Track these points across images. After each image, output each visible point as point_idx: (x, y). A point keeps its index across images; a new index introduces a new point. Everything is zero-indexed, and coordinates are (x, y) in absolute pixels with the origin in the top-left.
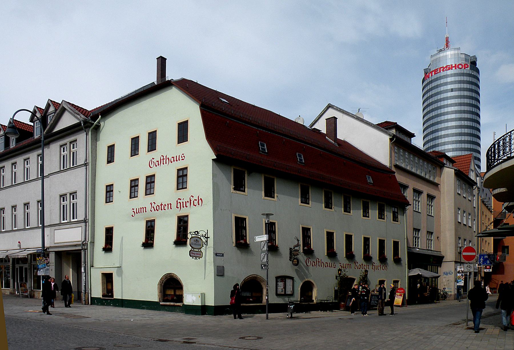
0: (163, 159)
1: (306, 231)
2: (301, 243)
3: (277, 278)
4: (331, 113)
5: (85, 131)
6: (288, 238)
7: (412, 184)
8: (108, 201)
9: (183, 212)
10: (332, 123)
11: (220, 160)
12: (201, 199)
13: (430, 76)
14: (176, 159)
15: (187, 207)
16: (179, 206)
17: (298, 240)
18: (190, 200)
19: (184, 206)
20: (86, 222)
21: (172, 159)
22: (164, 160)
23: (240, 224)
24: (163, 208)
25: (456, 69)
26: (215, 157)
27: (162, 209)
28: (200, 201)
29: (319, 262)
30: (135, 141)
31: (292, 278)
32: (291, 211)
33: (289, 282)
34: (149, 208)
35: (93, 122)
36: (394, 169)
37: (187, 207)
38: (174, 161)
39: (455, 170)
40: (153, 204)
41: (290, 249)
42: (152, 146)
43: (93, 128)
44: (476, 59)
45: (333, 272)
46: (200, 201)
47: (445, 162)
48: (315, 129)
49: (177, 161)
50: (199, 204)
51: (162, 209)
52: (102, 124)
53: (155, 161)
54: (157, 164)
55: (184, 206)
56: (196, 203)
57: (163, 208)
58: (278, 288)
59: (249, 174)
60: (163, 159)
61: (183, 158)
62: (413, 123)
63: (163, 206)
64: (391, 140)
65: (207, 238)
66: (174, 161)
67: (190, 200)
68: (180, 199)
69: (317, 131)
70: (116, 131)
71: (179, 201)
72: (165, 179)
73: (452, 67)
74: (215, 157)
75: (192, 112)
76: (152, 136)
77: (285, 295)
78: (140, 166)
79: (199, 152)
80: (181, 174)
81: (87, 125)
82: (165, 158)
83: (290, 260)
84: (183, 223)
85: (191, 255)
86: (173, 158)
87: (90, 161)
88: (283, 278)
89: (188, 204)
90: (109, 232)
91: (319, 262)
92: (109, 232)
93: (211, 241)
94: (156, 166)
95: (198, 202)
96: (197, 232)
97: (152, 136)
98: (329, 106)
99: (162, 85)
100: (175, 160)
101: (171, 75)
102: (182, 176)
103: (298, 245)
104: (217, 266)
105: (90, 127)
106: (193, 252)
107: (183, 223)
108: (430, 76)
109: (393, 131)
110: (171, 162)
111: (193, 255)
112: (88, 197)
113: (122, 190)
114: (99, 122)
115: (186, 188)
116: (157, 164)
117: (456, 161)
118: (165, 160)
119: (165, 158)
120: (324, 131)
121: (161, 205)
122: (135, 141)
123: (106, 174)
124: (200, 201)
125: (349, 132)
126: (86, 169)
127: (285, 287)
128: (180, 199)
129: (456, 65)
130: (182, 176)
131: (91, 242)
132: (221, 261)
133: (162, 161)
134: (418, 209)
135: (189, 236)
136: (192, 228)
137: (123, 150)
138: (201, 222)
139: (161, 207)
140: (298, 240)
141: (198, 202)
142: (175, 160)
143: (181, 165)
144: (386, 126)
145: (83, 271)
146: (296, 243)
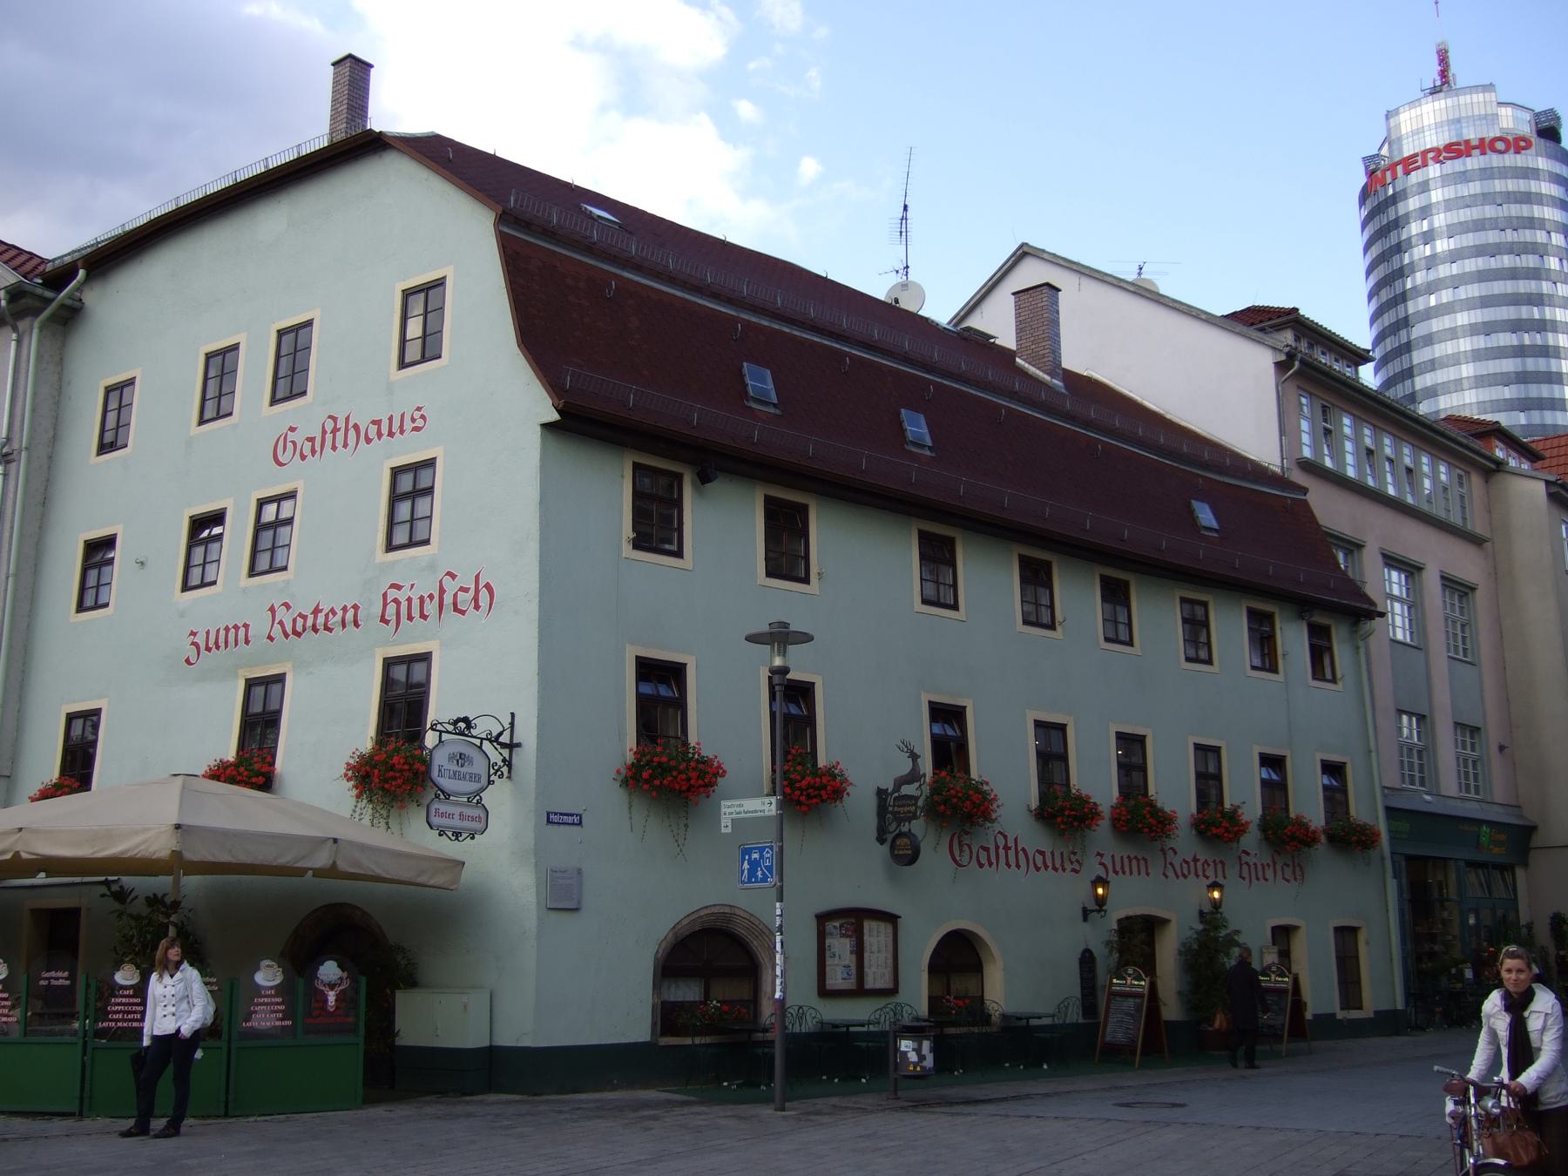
0: (335, 431)
1: (947, 715)
3: (823, 918)
4: (1030, 275)
5: (15, 329)
6: (871, 742)
8: (89, 602)
10: (1039, 306)
11: (576, 423)
12: (488, 586)
13: (1389, 179)
14: (387, 429)
15: (424, 617)
16: (392, 608)
17: (914, 757)
18: (442, 591)
21: (373, 429)
22: (339, 433)
23: (661, 683)
26: (554, 416)
28: (482, 594)
29: (1007, 848)
30: (221, 364)
31: (891, 919)
32: (888, 633)
33: (877, 936)
34: (261, 627)
35: (48, 294)
36: (1298, 477)
37: (424, 617)
38: (380, 435)
39: (1548, 483)
40: (281, 613)
41: (881, 793)
42: (289, 381)
45: (1072, 889)
46: (484, 594)
47: (1499, 453)
48: (969, 329)
49: (391, 434)
50: (477, 607)
52: (91, 297)
53: (298, 437)
54: (307, 451)
58: (829, 961)
59: (704, 478)
60: (335, 431)
61: (419, 423)
62: (1351, 319)
64: (1281, 367)
65: (511, 746)
66: (380, 435)
67: (442, 591)
68: (398, 587)
69: (980, 343)
70: (150, 331)
71: (392, 594)
72: (341, 507)
74: (554, 416)
75: (465, 251)
76: (293, 345)
77: (860, 991)
78: (232, 466)
79: (489, 401)
82: (341, 424)
83: (881, 840)
84: (403, 702)
86: (377, 423)
88: (854, 919)
89: (431, 608)
91: (1007, 848)
94: (303, 457)
95: (476, 599)
96: (466, 720)
97: (293, 345)
98: (1024, 253)
99: (356, 146)
100: (385, 430)
101: (391, 111)
102: (411, 487)
103: (914, 776)
105: (36, 312)
107: (403, 702)
108: (1389, 179)
109: (1288, 337)
110: (368, 441)
114: (79, 289)
116: (307, 451)
117: (1547, 454)
119: (341, 424)
120: (1006, 338)
121: (316, 611)
122: (221, 364)
123: (95, 495)
124: (484, 594)
125: (1100, 346)
128: (398, 587)
130: (411, 487)
133: (329, 437)
138: (486, 677)
140: (914, 757)
141: (476, 599)
142: (385, 430)
144: (1257, 321)
145: (865, 1029)
146: (905, 767)
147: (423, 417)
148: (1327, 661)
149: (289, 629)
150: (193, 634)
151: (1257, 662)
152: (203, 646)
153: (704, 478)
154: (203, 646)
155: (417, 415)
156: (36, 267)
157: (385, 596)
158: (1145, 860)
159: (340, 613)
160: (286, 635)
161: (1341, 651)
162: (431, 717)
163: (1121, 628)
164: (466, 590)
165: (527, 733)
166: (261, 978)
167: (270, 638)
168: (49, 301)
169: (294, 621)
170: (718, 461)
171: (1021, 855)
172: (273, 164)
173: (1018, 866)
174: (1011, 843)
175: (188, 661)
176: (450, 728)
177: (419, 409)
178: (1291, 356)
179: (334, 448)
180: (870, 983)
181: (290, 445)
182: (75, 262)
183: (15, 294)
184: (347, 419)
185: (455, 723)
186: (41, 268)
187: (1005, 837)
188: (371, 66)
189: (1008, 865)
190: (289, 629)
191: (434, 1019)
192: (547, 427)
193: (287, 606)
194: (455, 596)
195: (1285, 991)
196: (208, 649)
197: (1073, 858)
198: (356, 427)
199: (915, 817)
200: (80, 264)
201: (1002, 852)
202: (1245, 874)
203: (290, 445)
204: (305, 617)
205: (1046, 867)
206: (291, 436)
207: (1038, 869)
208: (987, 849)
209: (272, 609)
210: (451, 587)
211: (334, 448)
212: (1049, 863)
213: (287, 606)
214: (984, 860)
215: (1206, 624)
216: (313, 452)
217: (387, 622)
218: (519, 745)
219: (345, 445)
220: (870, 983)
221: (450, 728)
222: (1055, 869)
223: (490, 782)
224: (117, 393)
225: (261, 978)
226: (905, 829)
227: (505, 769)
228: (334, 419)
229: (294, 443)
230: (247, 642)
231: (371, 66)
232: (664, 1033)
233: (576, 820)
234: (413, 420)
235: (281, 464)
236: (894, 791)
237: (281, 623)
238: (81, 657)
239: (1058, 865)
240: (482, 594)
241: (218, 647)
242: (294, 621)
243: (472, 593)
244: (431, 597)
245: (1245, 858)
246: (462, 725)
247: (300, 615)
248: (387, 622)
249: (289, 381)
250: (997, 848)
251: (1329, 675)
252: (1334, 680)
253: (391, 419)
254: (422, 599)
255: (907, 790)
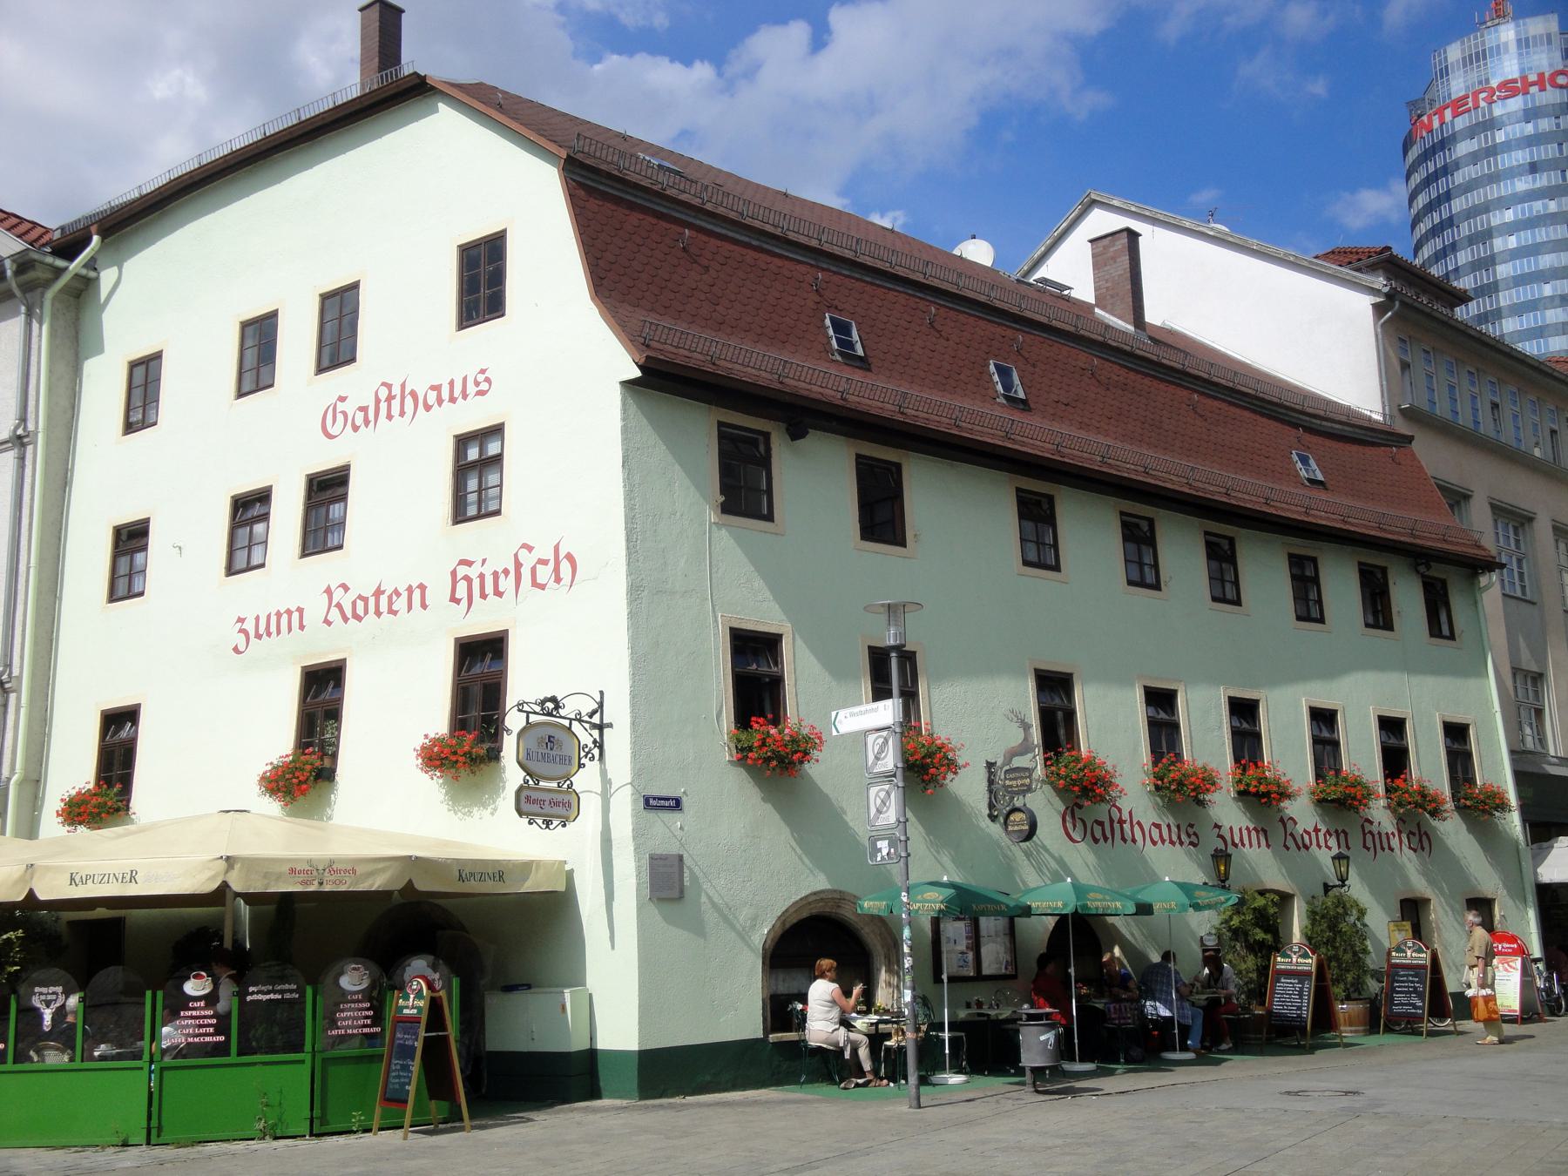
0: (390, 398)
2: (1036, 735)
7: (1486, 481)
9: (480, 623)
11: (661, 380)
12: (570, 557)
15: (498, 593)
16: (462, 589)
17: (1026, 727)
18: (518, 565)
19: (489, 589)
20: (23, 445)
21: (360, 417)
22: (396, 400)
24: (384, 606)
25: (1543, 89)
26: (636, 373)
27: (378, 613)
28: (563, 564)
34: (316, 608)
35: (60, 263)
37: (498, 593)
40: (338, 595)
41: (990, 765)
42: (337, 347)
43: (62, 291)
44: (570, 876)
46: (565, 567)
48: (1044, 281)
50: (558, 580)
51: (378, 613)
52: (107, 277)
53: (349, 407)
54: (359, 420)
55: (489, 589)
56: (544, 574)
57: (384, 606)
58: (944, 948)
60: (390, 398)
61: (484, 386)
63: (384, 600)
64: (1379, 309)
65: (601, 727)
66: (440, 401)
67: (518, 565)
68: (469, 563)
69: (1056, 293)
70: (165, 299)
71: (462, 571)
72: (399, 485)
73: (1527, 85)
74: (636, 373)
78: (279, 441)
79: (565, 358)
80: (473, 454)
81: (31, 275)
82: (396, 391)
84: (481, 659)
85: (525, 807)
86: (437, 388)
87: (39, 421)
89: (507, 584)
90: (119, 727)
91: (1121, 822)
92: (119, 727)
93: (619, 742)
94: (356, 428)
96: (553, 699)
99: (392, 94)
100: (445, 395)
102: (476, 469)
104: (652, 858)
105: (47, 284)
106: (535, 795)
107: (481, 659)
111: (535, 808)
112: (34, 359)
113: (189, 540)
114: (91, 264)
115: (497, 513)
118: (396, 404)
119: (396, 391)
120: (1083, 289)
121: (378, 593)
122: (259, 338)
123: (112, 475)
124: (565, 567)
126: (22, 459)
127: (976, 946)
128: (469, 563)
129: (1541, 76)
130: (476, 469)
131: (21, 784)
132: (668, 831)
133: (383, 406)
134: (1523, 588)
135: (514, 721)
136: (524, 683)
137: (201, 367)
138: (572, 654)
139: (379, 602)
140: (1026, 727)
142: (445, 395)
143: (473, 417)
146: (1016, 737)
147: (488, 380)
148: (1443, 618)
149: (349, 613)
150: (241, 620)
151: (1371, 620)
152: (252, 633)
153: (796, 433)
154: (252, 633)
155: (481, 378)
156: (41, 237)
157: (454, 573)
158: (1265, 832)
159: (405, 595)
160: (346, 619)
161: (1458, 603)
162: (511, 700)
163: (1228, 586)
164: (544, 562)
165: (619, 712)
166: (346, 982)
167: (328, 622)
168: (59, 272)
169: (354, 603)
170: (803, 416)
171: (1137, 828)
172: (237, 146)
173: (1134, 841)
174: (1125, 816)
175: (236, 650)
176: (538, 709)
177: (483, 371)
178: (1390, 297)
179: (390, 417)
180: (986, 971)
181: (340, 418)
182: (87, 228)
183: (24, 264)
184: (403, 386)
185: (543, 702)
186: (46, 238)
187: (1120, 810)
188: (403, 11)
189: (1124, 840)
190: (349, 613)
191: (520, 1026)
192: (628, 385)
193: (345, 588)
194: (534, 570)
195: (1424, 967)
196: (259, 636)
197: (1191, 831)
198: (414, 394)
199: (1029, 789)
200: (94, 229)
201: (1117, 826)
202: (1369, 843)
203: (340, 418)
204: (365, 600)
205: (1163, 841)
206: (341, 406)
207: (1154, 843)
208: (1101, 824)
209: (329, 591)
210: (528, 560)
211: (390, 417)
212: (1166, 836)
213: (345, 588)
214: (1098, 834)
215: (1316, 580)
216: (367, 422)
217: (458, 601)
218: (610, 725)
219: (402, 414)
220: (986, 971)
221: (538, 709)
222: (1172, 843)
223: (581, 766)
224: (143, 368)
225: (346, 982)
226: (1018, 802)
227: (596, 752)
228: (389, 386)
229: (345, 414)
230: (302, 627)
231: (403, 11)
232: (774, 1030)
233: (672, 803)
234: (477, 384)
235: (330, 437)
236: (1004, 765)
237: (339, 606)
238: (99, 656)
239: (1175, 838)
240: (563, 564)
241: (269, 634)
242: (354, 603)
243: (552, 565)
244: (506, 572)
245: (1368, 827)
246: (550, 705)
247: (360, 597)
248: (458, 601)
249: (337, 347)
250: (1112, 821)
251: (1445, 630)
252: (1452, 637)
253: (452, 383)
254: (496, 574)
255: (1018, 762)
